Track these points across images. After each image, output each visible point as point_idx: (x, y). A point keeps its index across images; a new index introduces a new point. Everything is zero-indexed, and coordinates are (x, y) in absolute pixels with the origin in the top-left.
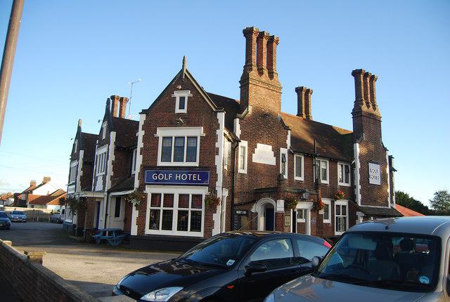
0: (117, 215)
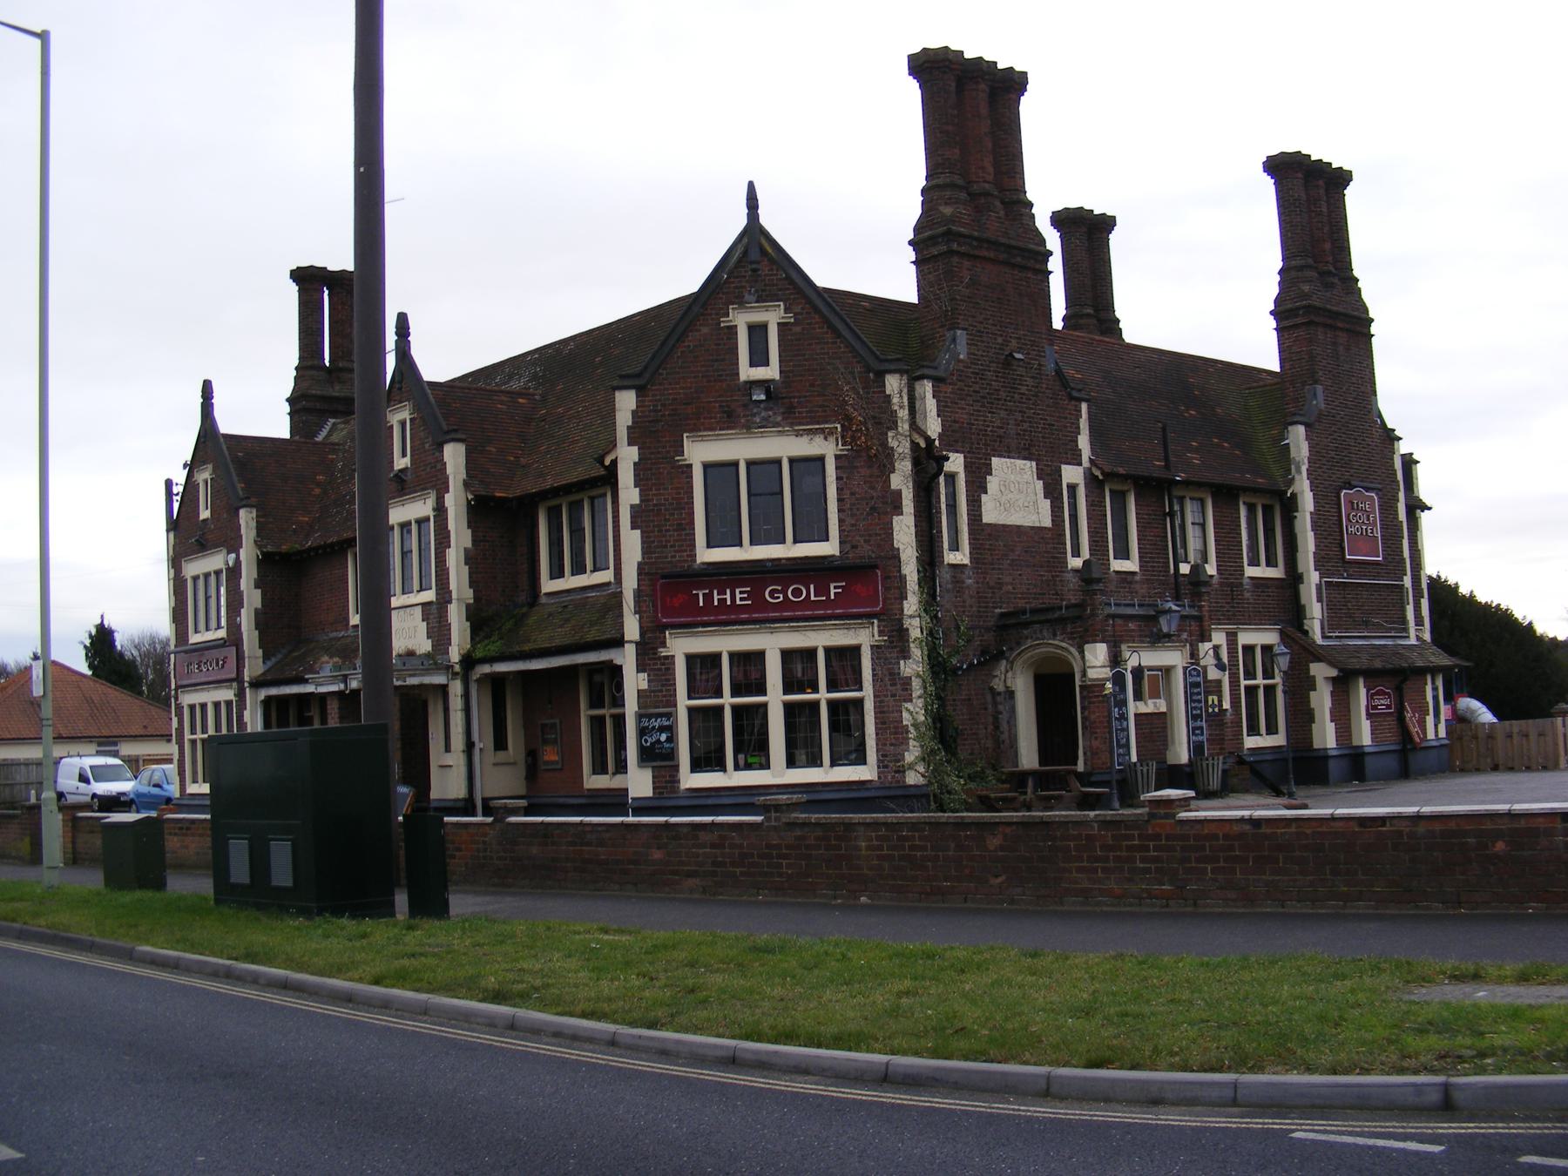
0: (500, 743)
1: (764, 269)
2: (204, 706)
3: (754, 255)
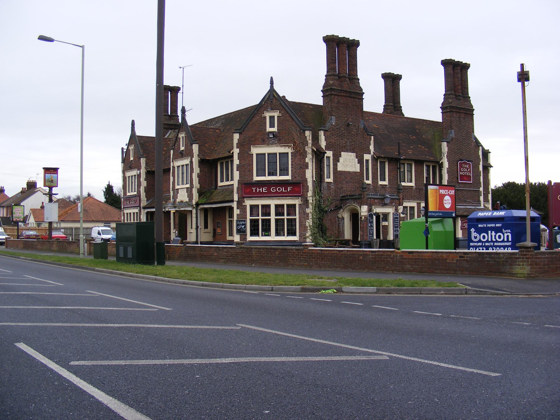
0: (206, 227)
1: (274, 101)
2: (130, 213)
3: (271, 97)
